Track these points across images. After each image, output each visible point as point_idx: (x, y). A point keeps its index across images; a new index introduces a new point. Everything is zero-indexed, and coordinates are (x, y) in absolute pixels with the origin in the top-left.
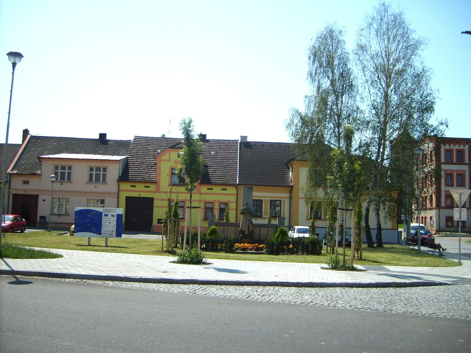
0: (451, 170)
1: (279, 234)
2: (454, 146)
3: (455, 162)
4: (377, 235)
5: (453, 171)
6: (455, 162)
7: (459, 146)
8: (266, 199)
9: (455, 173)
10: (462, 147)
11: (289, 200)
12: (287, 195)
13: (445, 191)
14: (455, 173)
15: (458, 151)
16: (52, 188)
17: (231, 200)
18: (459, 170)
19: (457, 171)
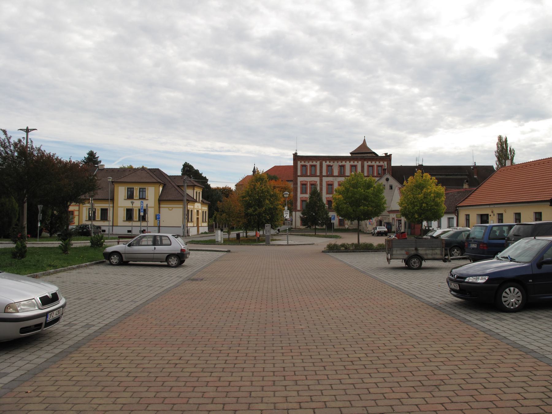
0: (305, 181)
1: (464, 255)
2: (375, 163)
3: (309, 174)
4: (371, 245)
5: (307, 182)
6: (309, 174)
7: (354, 162)
8: (136, 208)
9: (309, 183)
10: (314, 163)
11: (112, 208)
12: (112, 205)
13: (301, 198)
14: (309, 183)
15: (311, 166)
16: (359, 223)
17: (76, 209)
18: (312, 181)
19: (310, 182)
